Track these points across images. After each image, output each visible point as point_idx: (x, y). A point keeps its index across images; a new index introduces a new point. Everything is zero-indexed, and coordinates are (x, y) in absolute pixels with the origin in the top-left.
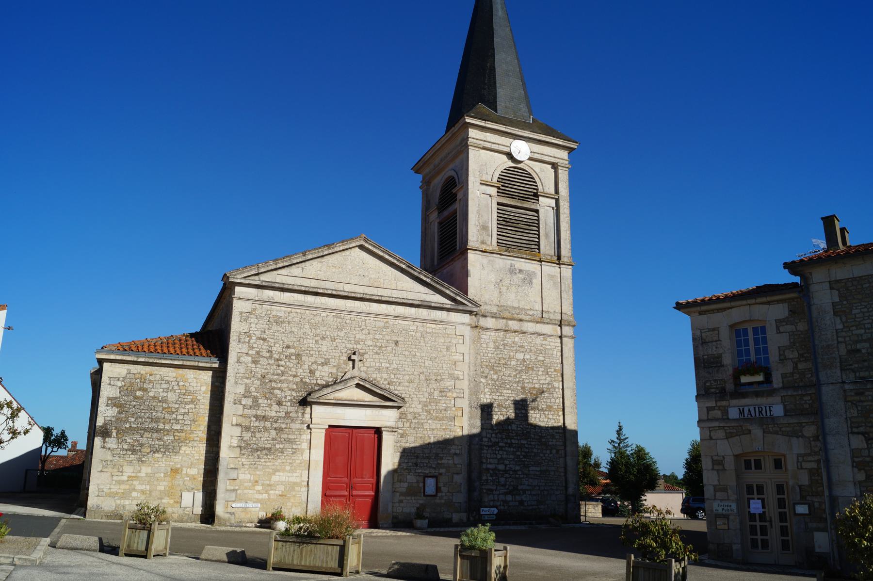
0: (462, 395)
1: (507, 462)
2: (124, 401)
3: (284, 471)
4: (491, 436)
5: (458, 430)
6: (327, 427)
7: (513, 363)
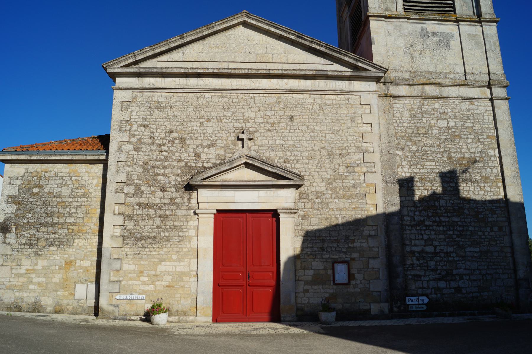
0: (374, 170)
1: (436, 243)
2: (22, 198)
3: (171, 260)
4: (415, 214)
5: (372, 209)
6: (215, 212)
7: (435, 131)
